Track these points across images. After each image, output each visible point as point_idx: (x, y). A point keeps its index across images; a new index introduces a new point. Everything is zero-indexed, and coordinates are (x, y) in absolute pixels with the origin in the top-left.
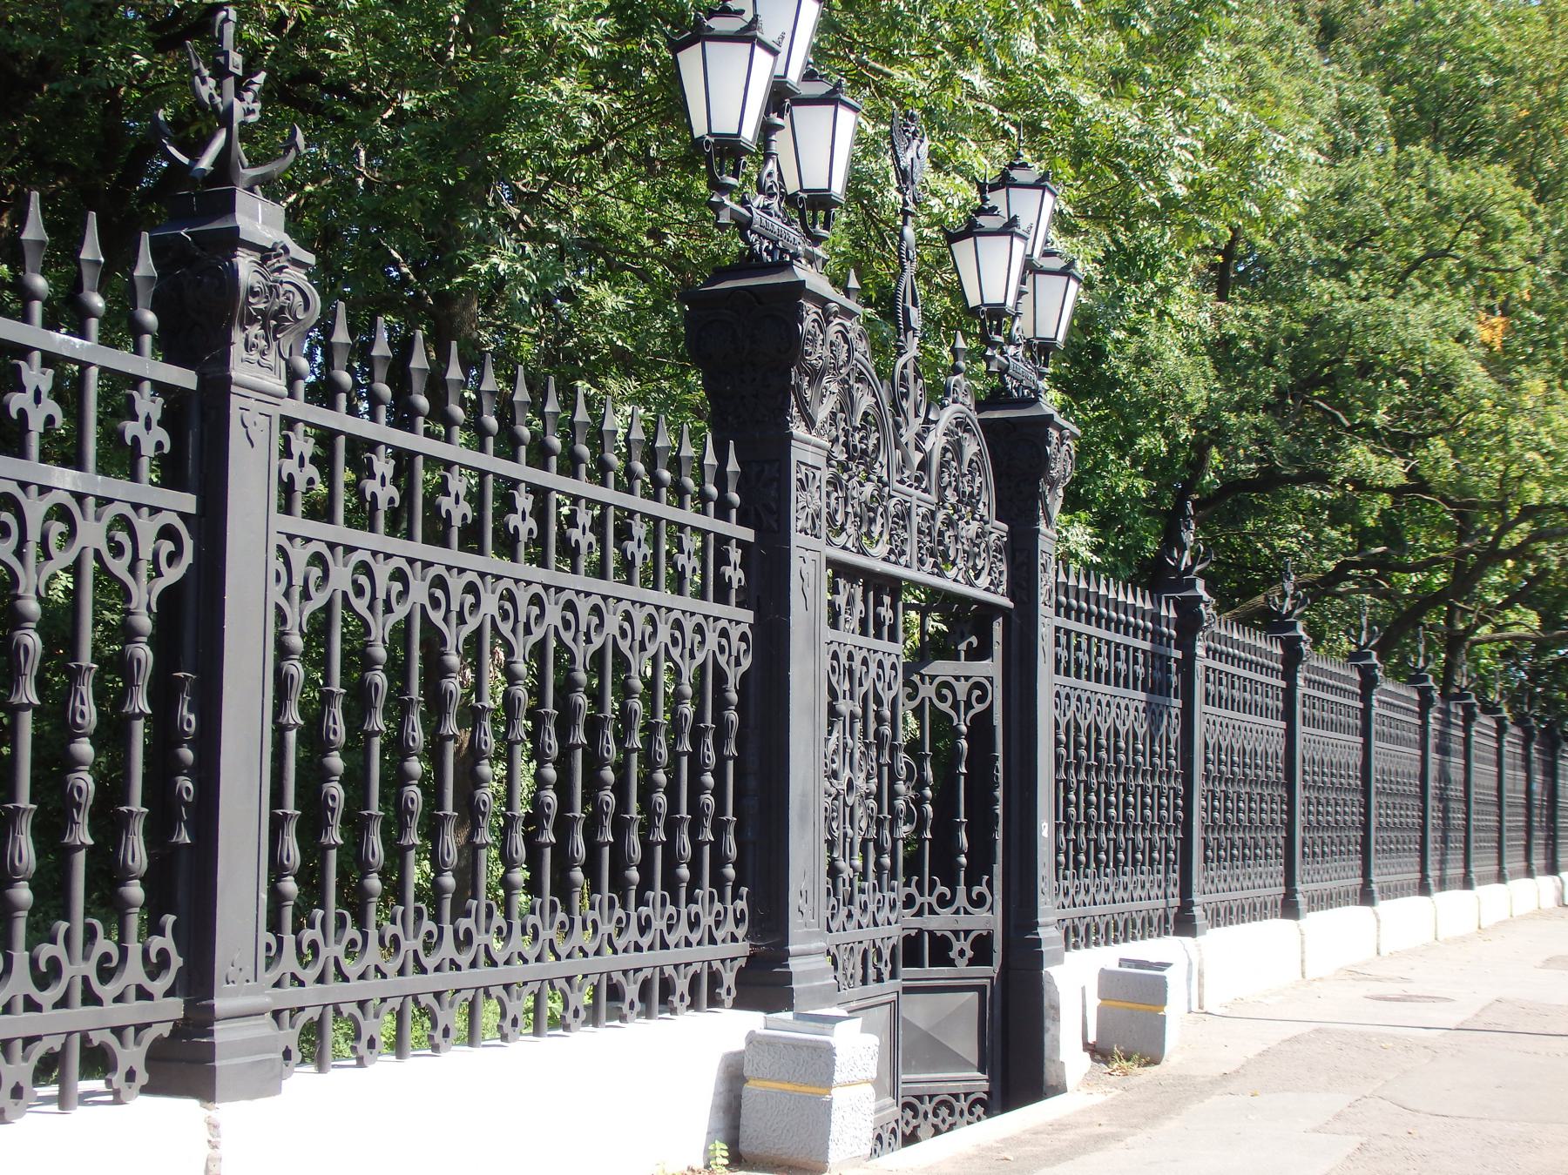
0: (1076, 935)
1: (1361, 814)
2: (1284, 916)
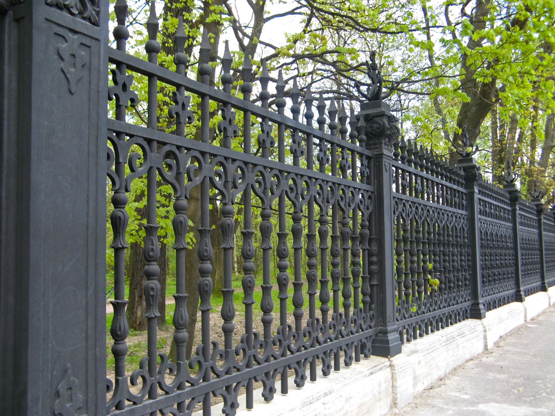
0: (431, 324)
1: (513, 259)
2: (516, 301)
